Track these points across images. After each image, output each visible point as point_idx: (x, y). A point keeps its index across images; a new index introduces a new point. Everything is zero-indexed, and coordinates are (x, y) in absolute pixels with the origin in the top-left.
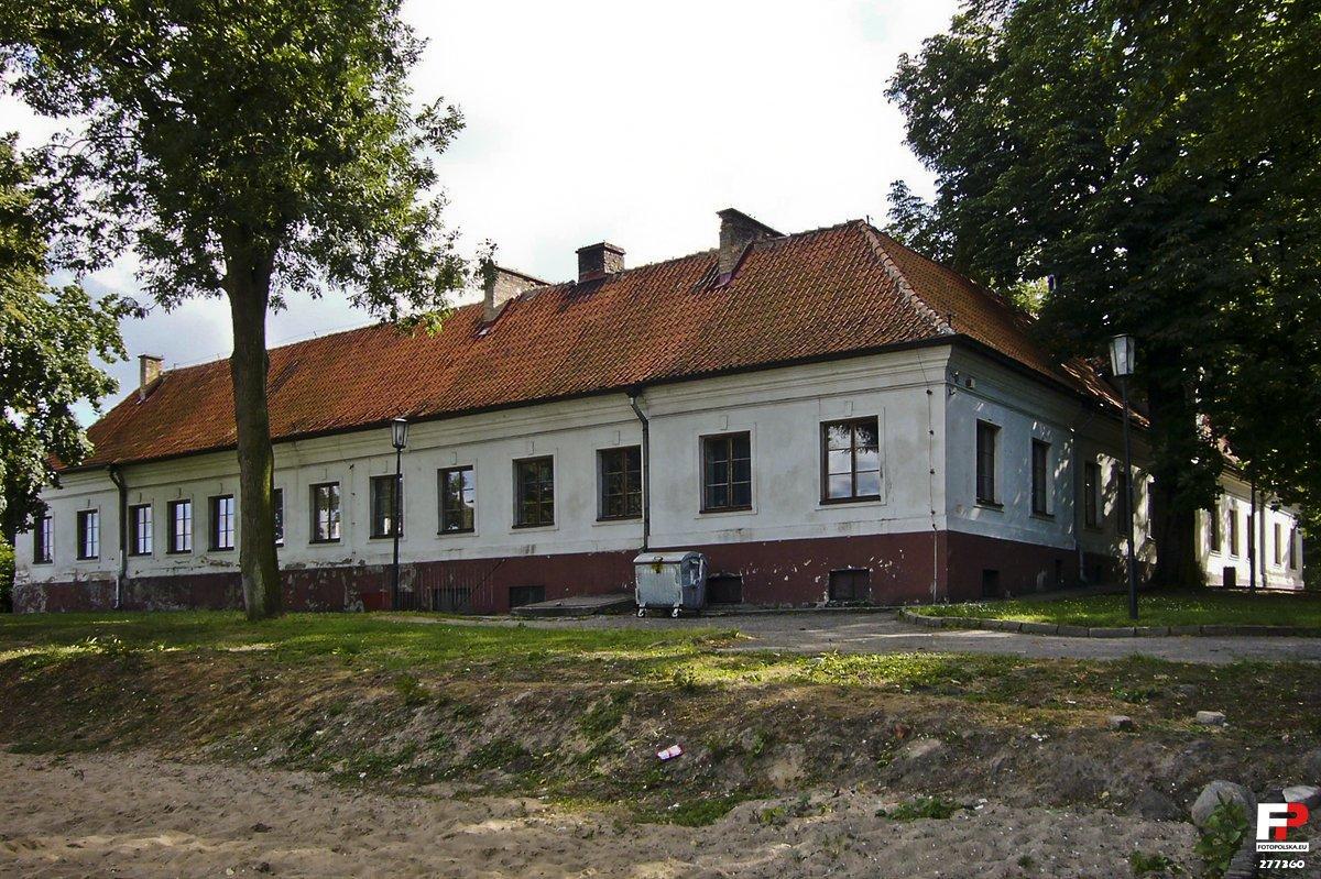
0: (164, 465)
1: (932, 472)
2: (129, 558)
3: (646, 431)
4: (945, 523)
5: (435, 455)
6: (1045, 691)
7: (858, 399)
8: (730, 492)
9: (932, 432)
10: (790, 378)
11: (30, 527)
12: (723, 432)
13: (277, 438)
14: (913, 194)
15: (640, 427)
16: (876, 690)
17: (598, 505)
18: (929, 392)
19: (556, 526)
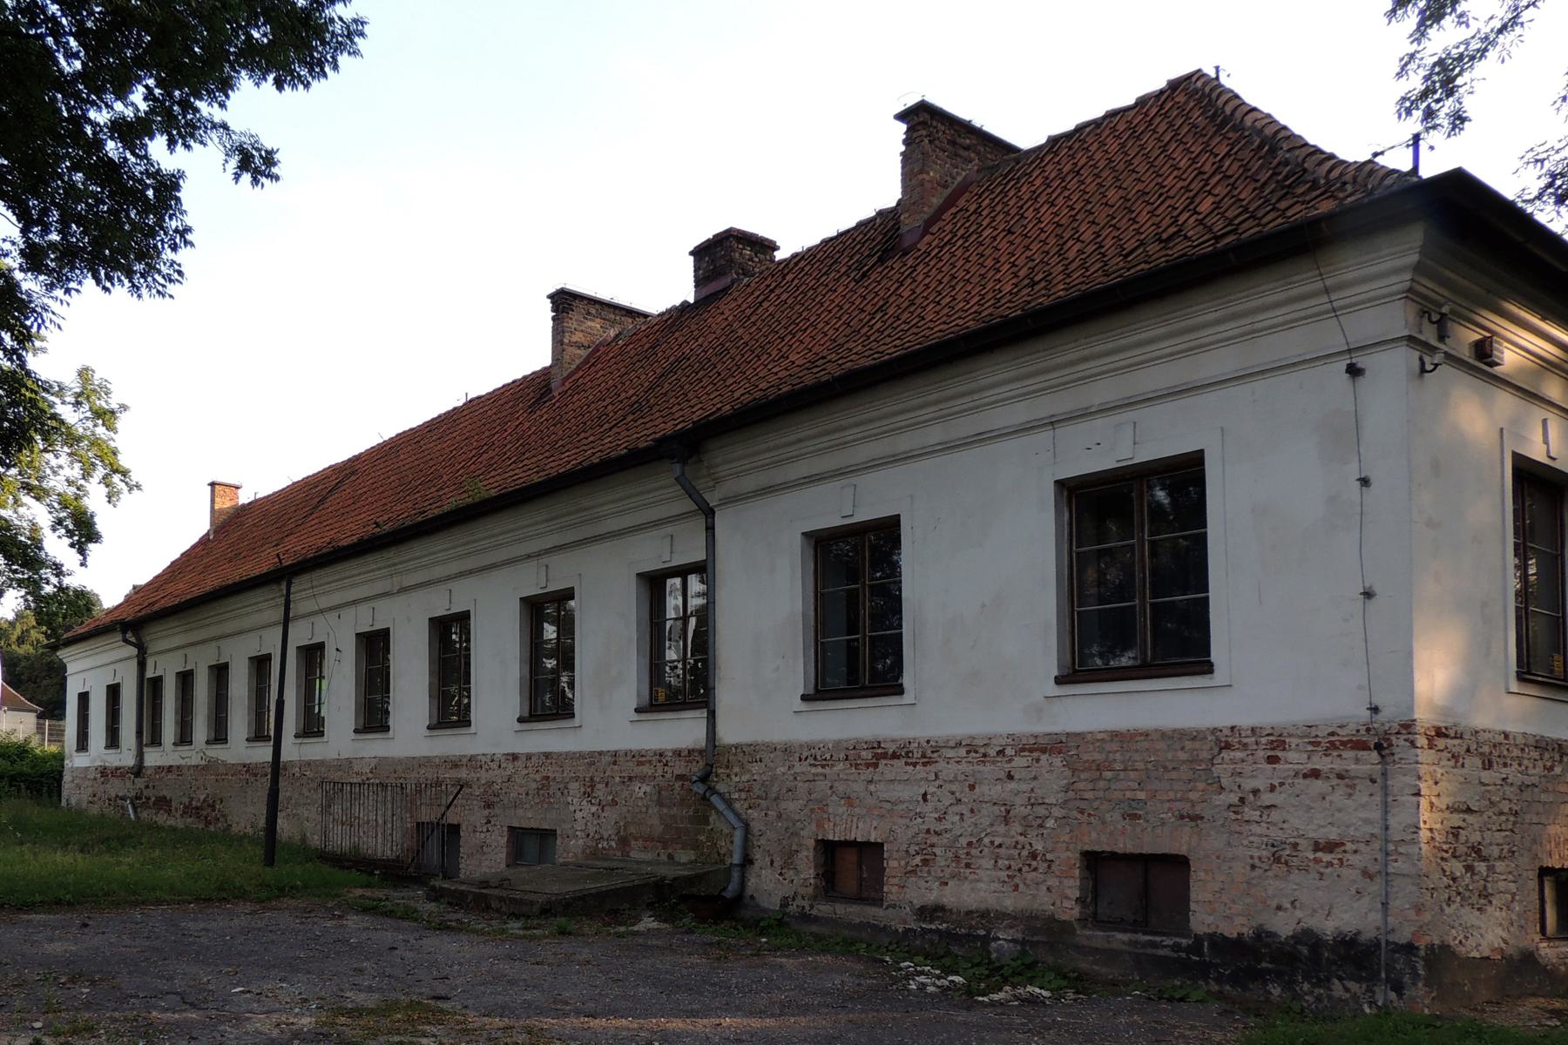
0: (418, 550)
1: (1368, 594)
2: (145, 749)
3: (710, 529)
4: (153, 764)
5: (349, 614)
6: (1175, 1027)
7: (1147, 415)
8: (1144, 623)
9: (1365, 482)
10: (983, 382)
11: (692, 615)
12: (666, 565)
13: (439, 517)
14: (50, 517)
15: (700, 523)
16: (534, 928)
17: (639, 681)
18: (1354, 371)
19: (577, 721)
